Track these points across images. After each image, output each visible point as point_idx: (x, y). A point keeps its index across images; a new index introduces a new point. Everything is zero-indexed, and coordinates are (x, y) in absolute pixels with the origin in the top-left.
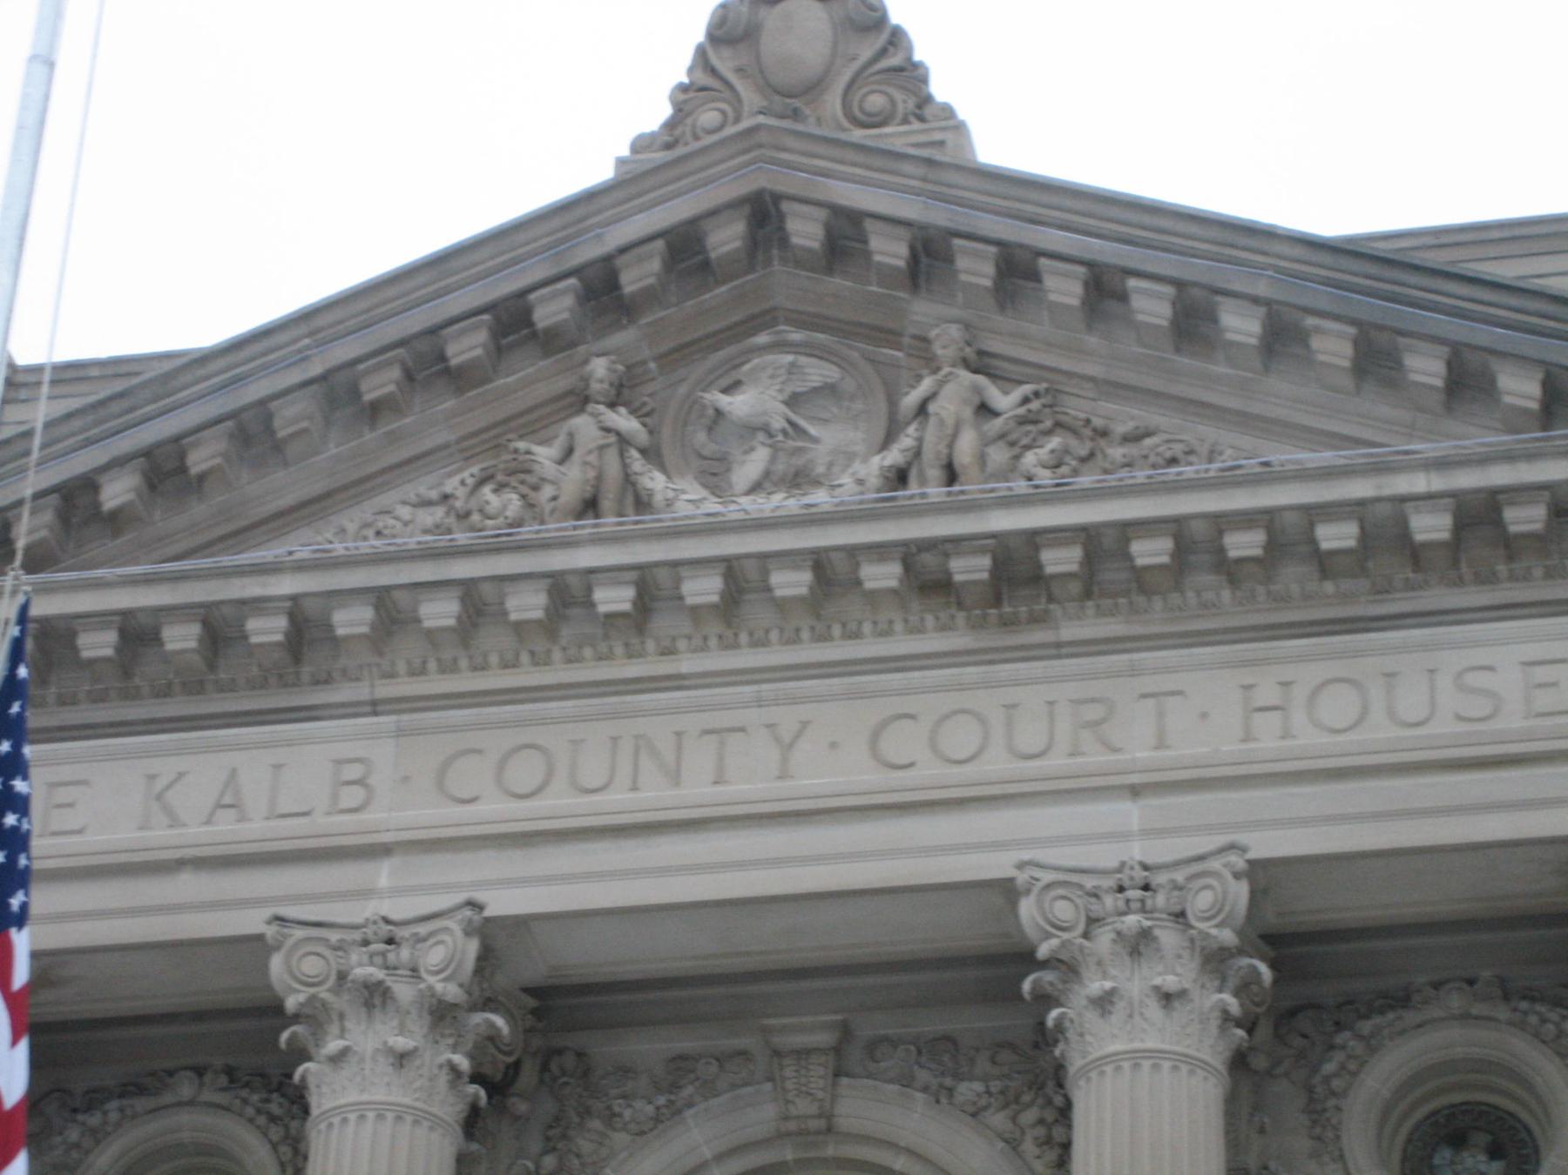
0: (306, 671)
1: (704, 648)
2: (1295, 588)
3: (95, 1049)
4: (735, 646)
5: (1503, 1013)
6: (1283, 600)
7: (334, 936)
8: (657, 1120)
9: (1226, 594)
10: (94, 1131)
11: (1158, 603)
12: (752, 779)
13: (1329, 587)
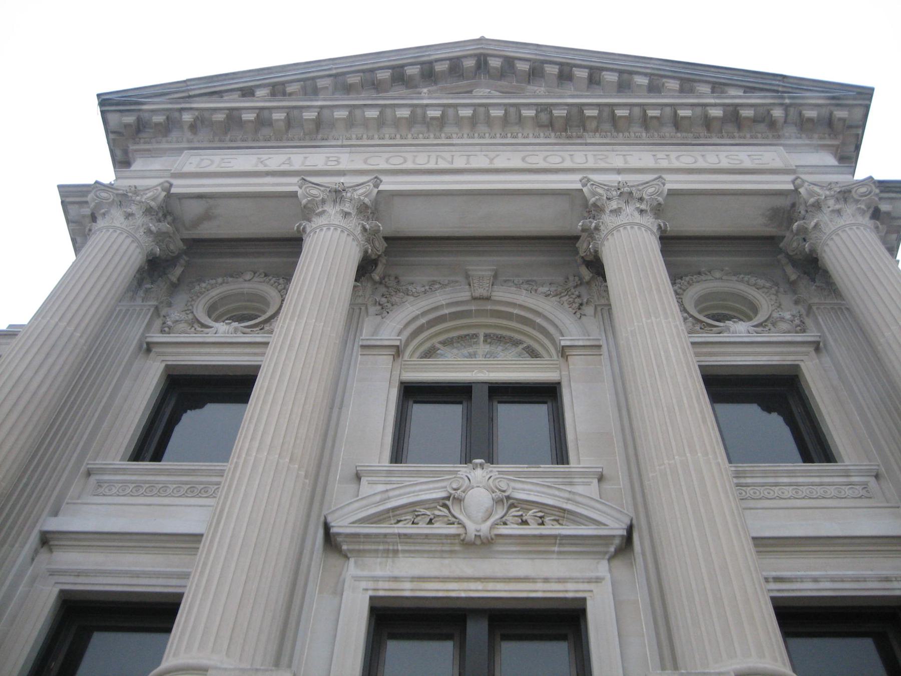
0: (320, 136)
1: (462, 137)
3: (83, 617)
4: (473, 138)
5: (735, 278)
6: (663, 137)
7: (322, 189)
9: (644, 134)
11: (621, 135)
12: (480, 161)
13: (679, 135)
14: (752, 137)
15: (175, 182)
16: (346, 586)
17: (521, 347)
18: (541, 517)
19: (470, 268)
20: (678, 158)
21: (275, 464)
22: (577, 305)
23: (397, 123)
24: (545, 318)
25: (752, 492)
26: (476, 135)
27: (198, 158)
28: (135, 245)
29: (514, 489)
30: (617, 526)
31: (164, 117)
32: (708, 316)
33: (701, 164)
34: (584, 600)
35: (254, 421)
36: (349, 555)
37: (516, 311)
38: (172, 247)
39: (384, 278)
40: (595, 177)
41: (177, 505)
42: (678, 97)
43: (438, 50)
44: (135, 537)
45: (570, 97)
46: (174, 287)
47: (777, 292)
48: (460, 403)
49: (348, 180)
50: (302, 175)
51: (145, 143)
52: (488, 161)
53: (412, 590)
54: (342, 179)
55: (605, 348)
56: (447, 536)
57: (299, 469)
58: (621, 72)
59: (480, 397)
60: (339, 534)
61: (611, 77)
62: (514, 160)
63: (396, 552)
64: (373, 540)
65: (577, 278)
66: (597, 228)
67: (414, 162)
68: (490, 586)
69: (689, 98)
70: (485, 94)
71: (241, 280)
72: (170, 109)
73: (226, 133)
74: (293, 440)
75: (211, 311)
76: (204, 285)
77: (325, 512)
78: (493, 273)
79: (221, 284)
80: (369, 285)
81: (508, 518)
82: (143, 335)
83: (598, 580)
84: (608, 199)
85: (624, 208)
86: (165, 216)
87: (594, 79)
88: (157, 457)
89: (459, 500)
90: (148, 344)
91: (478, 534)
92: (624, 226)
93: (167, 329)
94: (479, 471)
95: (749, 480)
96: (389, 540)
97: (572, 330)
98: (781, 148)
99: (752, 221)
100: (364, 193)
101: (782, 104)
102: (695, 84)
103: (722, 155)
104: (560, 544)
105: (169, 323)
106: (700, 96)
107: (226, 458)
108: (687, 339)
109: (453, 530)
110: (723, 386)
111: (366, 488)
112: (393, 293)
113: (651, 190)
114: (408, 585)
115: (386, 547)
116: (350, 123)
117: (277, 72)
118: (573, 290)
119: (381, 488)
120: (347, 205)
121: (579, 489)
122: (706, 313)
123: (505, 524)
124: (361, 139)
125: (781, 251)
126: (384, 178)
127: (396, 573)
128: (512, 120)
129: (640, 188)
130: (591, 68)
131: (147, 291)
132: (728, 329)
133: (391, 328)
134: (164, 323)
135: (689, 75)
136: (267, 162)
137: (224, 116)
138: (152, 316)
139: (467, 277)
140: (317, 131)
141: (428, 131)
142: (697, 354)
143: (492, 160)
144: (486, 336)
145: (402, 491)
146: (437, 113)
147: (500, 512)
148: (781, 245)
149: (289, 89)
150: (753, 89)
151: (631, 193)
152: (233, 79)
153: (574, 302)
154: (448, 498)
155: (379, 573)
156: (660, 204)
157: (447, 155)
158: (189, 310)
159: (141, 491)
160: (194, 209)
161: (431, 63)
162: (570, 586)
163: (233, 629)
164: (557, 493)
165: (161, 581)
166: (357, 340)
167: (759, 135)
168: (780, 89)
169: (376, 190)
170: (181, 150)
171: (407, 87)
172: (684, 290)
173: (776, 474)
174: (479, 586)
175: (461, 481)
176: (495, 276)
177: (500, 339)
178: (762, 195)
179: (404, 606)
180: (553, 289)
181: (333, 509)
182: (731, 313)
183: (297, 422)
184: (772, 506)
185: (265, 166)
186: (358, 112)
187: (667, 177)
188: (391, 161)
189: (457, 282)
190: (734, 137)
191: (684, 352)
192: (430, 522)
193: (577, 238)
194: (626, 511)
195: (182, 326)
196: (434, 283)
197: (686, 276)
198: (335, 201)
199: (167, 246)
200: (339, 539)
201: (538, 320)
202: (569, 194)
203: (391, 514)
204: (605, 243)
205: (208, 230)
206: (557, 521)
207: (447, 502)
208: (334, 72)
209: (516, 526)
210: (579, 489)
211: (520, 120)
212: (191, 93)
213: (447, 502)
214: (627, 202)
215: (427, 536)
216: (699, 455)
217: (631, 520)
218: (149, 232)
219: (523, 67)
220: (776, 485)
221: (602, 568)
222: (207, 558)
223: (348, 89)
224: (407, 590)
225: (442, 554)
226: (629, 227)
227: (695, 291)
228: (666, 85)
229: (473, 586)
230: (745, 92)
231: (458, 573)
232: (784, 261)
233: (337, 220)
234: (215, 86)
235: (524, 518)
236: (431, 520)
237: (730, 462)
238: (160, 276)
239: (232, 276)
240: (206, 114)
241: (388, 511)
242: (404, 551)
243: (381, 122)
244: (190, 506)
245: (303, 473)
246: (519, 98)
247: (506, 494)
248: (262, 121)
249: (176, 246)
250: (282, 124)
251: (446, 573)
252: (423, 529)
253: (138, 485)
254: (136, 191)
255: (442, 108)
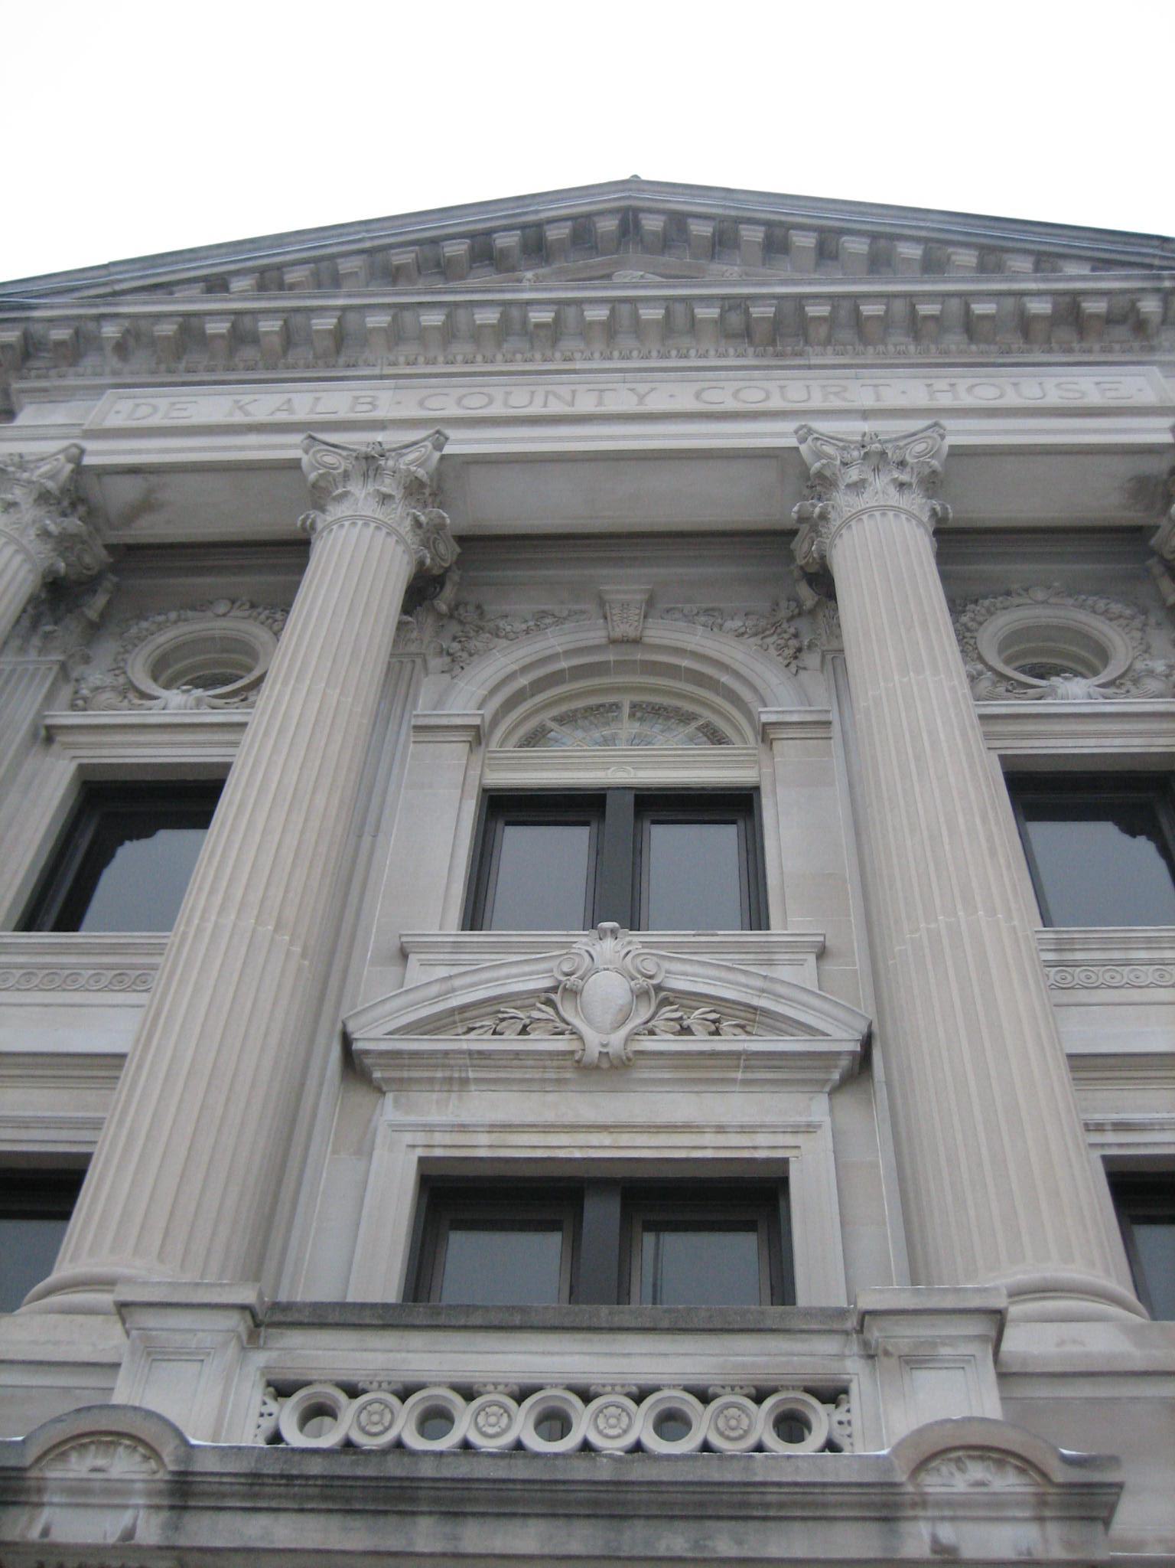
0: (342, 360)
2: (953, 347)
5: (1070, 601)
6: (947, 353)
7: (344, 453)
8: (527, 631)
9: (912, 348)
10: (160, 624)
11: (870, 349)
12: (621, 400)
13: (974, 347)
14: (1103, 350)
15: (89, 445)
16: (379, 1140)
17: (694, 725)
18: (714, 1022)
19: (607, 588)
20: (970, 389)
21: (248, 935)
22: (792, 651)
23: (477, 334)
24: (737, 675)
25: (1107, 976)
26: (616, 354)
27: (130, 403)
28: (19, 558)
29: (668, 972)
30: (845, 1036)
31: (71, 331)
32: (1022, 670)
33: (1012, 400)
34: (785, 1162)
35: (215, 863)
36: (385, 1089)
37: (685, 663)
38: (87, 559)
39: (457, 607)
40: (822, 426)
41: (92, 1006)
42: (972, 280)
43: (552, 202)
44: (21, 1060)
45: (782, 283)
46: (94, 630)
47: (1145, 625)
48: (733, 822)
49: (388, 438)
50: (309, 429)
51: (39, 377)
52: (635, 399)
53: (490, 1146)
54: (380, 437)
55: (836, 727)
56: (552, 1055)
57: (291, 942)
58: (874, 236)
59: (620, 812)
60: (367, 1052)
61: (857, 246)
62: (677, 396)
63: (465, 1082)
64: (425, 1061)
65: (793, 604)
66: (823, 517)
67: (506, 404)
68: (625, 1139)
69: (993, 281)
70: (638, 282)
71: (209, 614)
72: (79, 317)
73: (179, 358)
74: (281, 895)
75: (156, 672)
76: (144, 624)
77: (343, 1015)
78: (646, 597)
79: (176, 622)
80: (430, 620)
81: (658, 1023)
82: (39, 715)
83: (810, 1129)
84: (845, 464)
85: (871, 479)
86: (73, 505)
87: (827, 251)
88: (70, 919)
89: (574, 993)
90: (49, 728)
91: (605, 1050)
92: (869, 511)
93: (80, 703)
94: (609, 943)
95: (1079, 956)
96: (452, 1062)
97: (781, 696)
98: (1155, 368)
99: (1102, 500)
100: (419, 460)
101: (1158, 290)
102: (1006, 256)
103: (1050, 384)
104: (746, 1067)
105: (85, 692)
106: (1015, 276)
107: (167, 924)
108: (970, 710)
109: (561, 1044)
110: (1043, 792)
111: (416, 972)
112: (472, 634)
113: (920, 447)
114: (484, 1139)
115: (447, 1074)
116: (395, 336)
117: (271, 247)
118: (785, 626)
119: (442, 972)
120: (387, 481)
121: (784, 973)
122: (1017, 664)
123: (652, 1033)
124: (414, 363)
125: (1152, 553)
126: (451, 433)
127: (465, 1118)
128: (677, 327)
129: (901, 444)
130: (820, 230)
131: (47, 636)
132: (1053, 692)
133: (466, 696)
134: (76, 692)
135: (995, 240)
136: (249, 408)
137: (175, 327)
138: (56, 679)
139: (602, 603)
140: (339, 351)
141: (532, 348)
142: (988, 736)
143: (641, 398)
144: (634, 706)
145: (476, 978)
146: (546, 316)
147: (644, 1013)
148: (1153, 542)
149: (292, 276)
150: (1109, 264)
151: (883, 454)
152: (190, 261)
153: (786, 646)
154: (554, 989)
155: (434, 1118)
156: (934, 472)
157: (565, 391)
158: (119, 669)
159: (35, 981)
160: (126, 491)
161: (539, 225)
162: (761, 1139)
163: (172, 1213)
164: (742, 979)
165: (65, 1134)
166: (406, 717)
167: (1117, 347)
168: (1157, 262)
169: (437, 455)
170: (100, 390)
171: (499, 271)
172: (981, 624)
173: (1126, 944)
174: (606, 1139)
175: (577, 959)
176: (650, 603)
177: (658, 712)
178: (1116, 453)
179: (520, 1174)
180: (749, 623)
181: (359, 1008)
182: (1066, 663)
183: (290, 860)
184: (1117, 1000)
185: (247, 414)
186: (408, 316)
187: (949, 424)
188: (466, 402)
189: (582, 612)
190: (1070, 351)
191: (964, 734)
192: (524, 1031)
193: (793, 533)
194: (862, 1012)
195: (107, 697)
196: (544, 614)
197: (986, 598)
198: (365, 476)
199: (79, 558)
200: (368, 1061)
201: (725, 679)
202: (776, 457)
203: (457, 1018)
204: (837, 541)
205: (151, 529)
206: (742, 1027)
207: (553, 996)
208: (368, 245)
209: (672, 1037)
210: (784, 973)
211: (693, 326)
212: (117, 287)
213: (553, 996)
214: (876, 470)
215: (517, 1054)
216: (981, 913)
217: (870, 1026)
218: (45, 534)
219: (701, 230)
220: (1127, 963)
221: (818, 1108)
222: (130, 1096)
223: (393, 275)
224: (482, 1146)
225: (542, 1085)
226: (877, 514)
227: (997, 626)
228: (954, 258)
229: (595, 1139)
230: (1093, 269)
231: (570, 1118)
232: (1158, 570)
233: (369, 508)
234: (159, 274)
235: (685, 1023)
236: (525, 1027)
237: (1046, 920)
238: (70, 611)
239: (193, 608)
240: (143, 324)
241: (452, 1011)
242: (478, 1080)
243: (449, 334)
244: (21, 1005)
245: (297, 949)
246: (695, 286)
247: (654, 982)
248: (241, 336)
249: (96, 557)
250: (276, 341)
251: (550, 1117)
252: (511, 1042)
253: (29, 972)
254: (22, 463)
255: (555, 307)
